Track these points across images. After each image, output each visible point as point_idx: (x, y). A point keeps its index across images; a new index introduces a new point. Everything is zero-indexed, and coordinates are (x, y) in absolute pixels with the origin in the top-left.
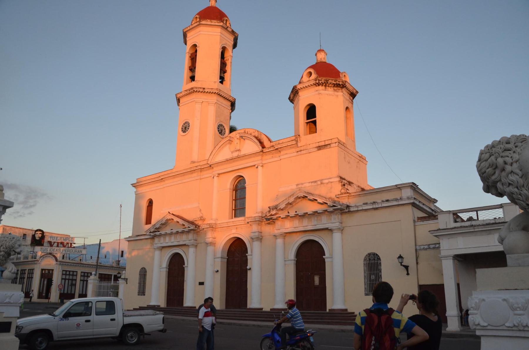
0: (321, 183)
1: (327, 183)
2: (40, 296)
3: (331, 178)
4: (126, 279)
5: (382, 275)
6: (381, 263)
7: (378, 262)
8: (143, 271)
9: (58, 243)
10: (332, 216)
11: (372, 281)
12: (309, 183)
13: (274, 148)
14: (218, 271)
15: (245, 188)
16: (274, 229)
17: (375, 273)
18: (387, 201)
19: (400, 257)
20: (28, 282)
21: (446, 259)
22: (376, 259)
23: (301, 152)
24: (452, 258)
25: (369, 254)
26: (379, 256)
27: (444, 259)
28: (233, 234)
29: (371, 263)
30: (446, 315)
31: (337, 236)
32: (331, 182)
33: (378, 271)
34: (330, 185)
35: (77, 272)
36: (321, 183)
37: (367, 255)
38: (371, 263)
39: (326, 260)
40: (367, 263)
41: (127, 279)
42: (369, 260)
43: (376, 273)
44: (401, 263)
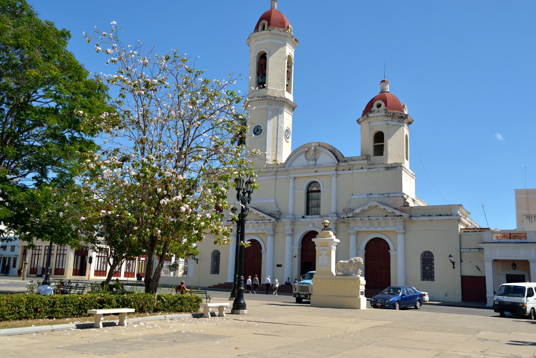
0: (388, 196)
1: (393, 197)
2: (75, 273)
3: (396, 193)
9: (220, 315)
12: (378, 194)
14: (296, 256)
19: (450, 256)
20: (140, 268)
22: (430, 255)
25: (425, 252)
28: (310, 228)
30: (487, 296)
34: (395, 198)
35: (46, 246)
36: (388, 196)
37: (423, 252)
39: (391, 254)
41: (197, 259)
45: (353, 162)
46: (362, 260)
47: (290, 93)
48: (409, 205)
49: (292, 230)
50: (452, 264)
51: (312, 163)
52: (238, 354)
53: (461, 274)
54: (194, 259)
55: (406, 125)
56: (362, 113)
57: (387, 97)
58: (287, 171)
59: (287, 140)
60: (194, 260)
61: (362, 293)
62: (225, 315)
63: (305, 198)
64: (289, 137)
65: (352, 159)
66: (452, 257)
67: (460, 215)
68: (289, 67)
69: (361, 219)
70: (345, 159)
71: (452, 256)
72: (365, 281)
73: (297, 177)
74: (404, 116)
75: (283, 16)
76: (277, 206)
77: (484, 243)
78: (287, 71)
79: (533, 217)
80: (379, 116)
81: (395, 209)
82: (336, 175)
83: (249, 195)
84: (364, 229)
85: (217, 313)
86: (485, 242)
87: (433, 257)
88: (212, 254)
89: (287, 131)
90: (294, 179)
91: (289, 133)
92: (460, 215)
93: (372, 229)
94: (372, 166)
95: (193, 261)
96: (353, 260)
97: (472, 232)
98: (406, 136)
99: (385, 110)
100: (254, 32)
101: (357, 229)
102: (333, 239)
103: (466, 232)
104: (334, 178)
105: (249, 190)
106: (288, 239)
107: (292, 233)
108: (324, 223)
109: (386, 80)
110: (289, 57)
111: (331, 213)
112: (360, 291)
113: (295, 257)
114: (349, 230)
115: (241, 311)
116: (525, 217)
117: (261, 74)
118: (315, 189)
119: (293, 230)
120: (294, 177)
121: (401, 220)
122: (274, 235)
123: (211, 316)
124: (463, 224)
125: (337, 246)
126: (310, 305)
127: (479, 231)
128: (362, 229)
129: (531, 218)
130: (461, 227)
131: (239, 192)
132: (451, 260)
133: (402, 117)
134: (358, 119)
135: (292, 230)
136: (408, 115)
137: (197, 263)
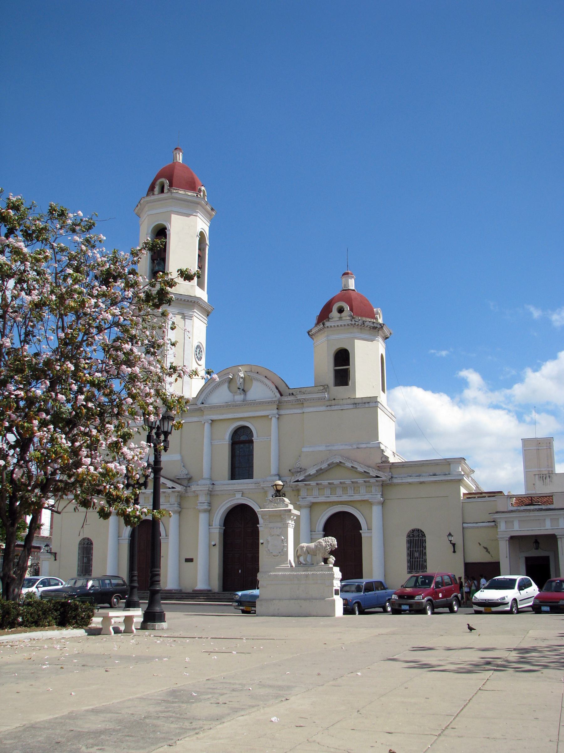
4: (54, 554)
5: (427, 553)
6: (425, 540)
7: (422, 539)
8: (86, 543)
10: (373, 487)
11: (416, 559)
13: (297, 397)
14: (215, 545)
15: (251, 442)
16: (299, 497)
17: (419, 550)
18: (435, 475)
19: (450, 534)
21: (502, 540)
23: (331, 407)
24: (508, 539)
25: (413, 531)
26: (423, 532)
27: (501, 540)
29: (415, 539)
31: (376, 511)
32: (370, 448)
33: (422, 548)
36: (358, 448)
37: (410, 531)
38: (415, 539)
40: (410, 539)
41: (56, 553)
42: (413, 536)
43: (415, 548)
44: (451, 541)
45: (303, 397)
46: (336, 540)
47: (204, 291)
48: (389, 460)
49: (209, 503)
50: (451, 546)
51: (239, 397)
52: (207, 679)
53: (464, 561)
54: (51, 553)
55: (380, 340)
56: (315, 321)
57: (353, 298)
58: (200, 410)
59: (199, 362)
60: (49, 554)
61: (337, 593)
62: (135, 630)
63: (229, 452)
64: (201, 358)
65: (301, 391)
66: (452, 536)
67: (462, 473)
68: (201, 249)
69: (317, 484)
70: (291, 392)
71: (452, 534)
72: (340, 574)
73: (215, 420)
74: (379, 326)
75: (192, 173)
76: (183, 466)
77: (497, 512)
78: (199, 256)
79: (548, 477)
80: (341, 325)
81: (369, 467)
82: (277, 416)
83: (166, 437)
84: (322, 499)
85: (122, 628)
86: (498, 510)
87: (425, 537)
88: (80, 544)
89: (198, 347)
90: (211, 423)
91: (201, 352)
92: (462, 473)
93: (334, 499)
94: (333, 402)
95: (49, 556)
96: (322, 541)
97: (478, 497)
98: (382, 356)
99: (351, 316)
100: (147, 195)
101: (311, 499)
102: (290, 510)
103: (470, 498)
104: (274, 420)
105: (166, 429)
106: (203, 517)
107: (209, 508)
108: (276, 485)
109: (349, 272)
110: (202, 234)
111: (271, 476)
112: (334, 588)
113: (214, 545)
114: (299, 501)
115: (158, 625)
116: (537, 477)
117: (157, 260)
118: (243, 438)
119: (210, 504)
120: (212, 420)
121: (377, 483)
122: (180, 513)
123: (115, 633)
124: (467, 487)
125: (296, 521)
126: (255, 615)
127: (489, 497)
128: (320, 498)
129: (546, 478)
130: (463, 491)
131: (151, 431)
132: (451, 541)
133: (375, 328)
134: (309, 329)
135: (209, 503)
136: (384, 324)
137: (55, 560)
